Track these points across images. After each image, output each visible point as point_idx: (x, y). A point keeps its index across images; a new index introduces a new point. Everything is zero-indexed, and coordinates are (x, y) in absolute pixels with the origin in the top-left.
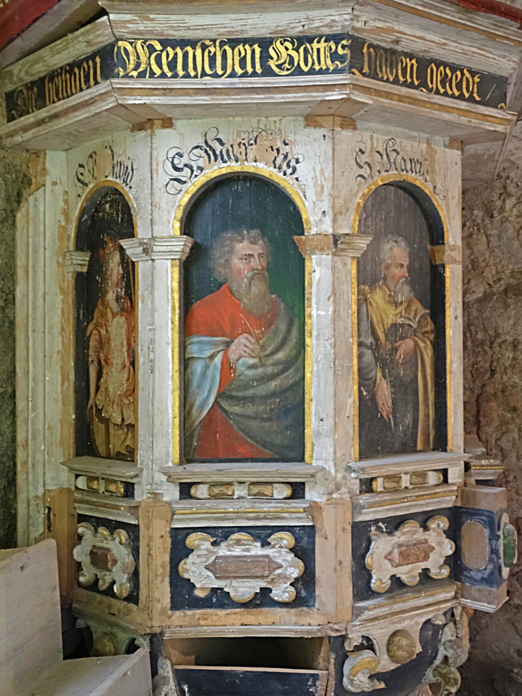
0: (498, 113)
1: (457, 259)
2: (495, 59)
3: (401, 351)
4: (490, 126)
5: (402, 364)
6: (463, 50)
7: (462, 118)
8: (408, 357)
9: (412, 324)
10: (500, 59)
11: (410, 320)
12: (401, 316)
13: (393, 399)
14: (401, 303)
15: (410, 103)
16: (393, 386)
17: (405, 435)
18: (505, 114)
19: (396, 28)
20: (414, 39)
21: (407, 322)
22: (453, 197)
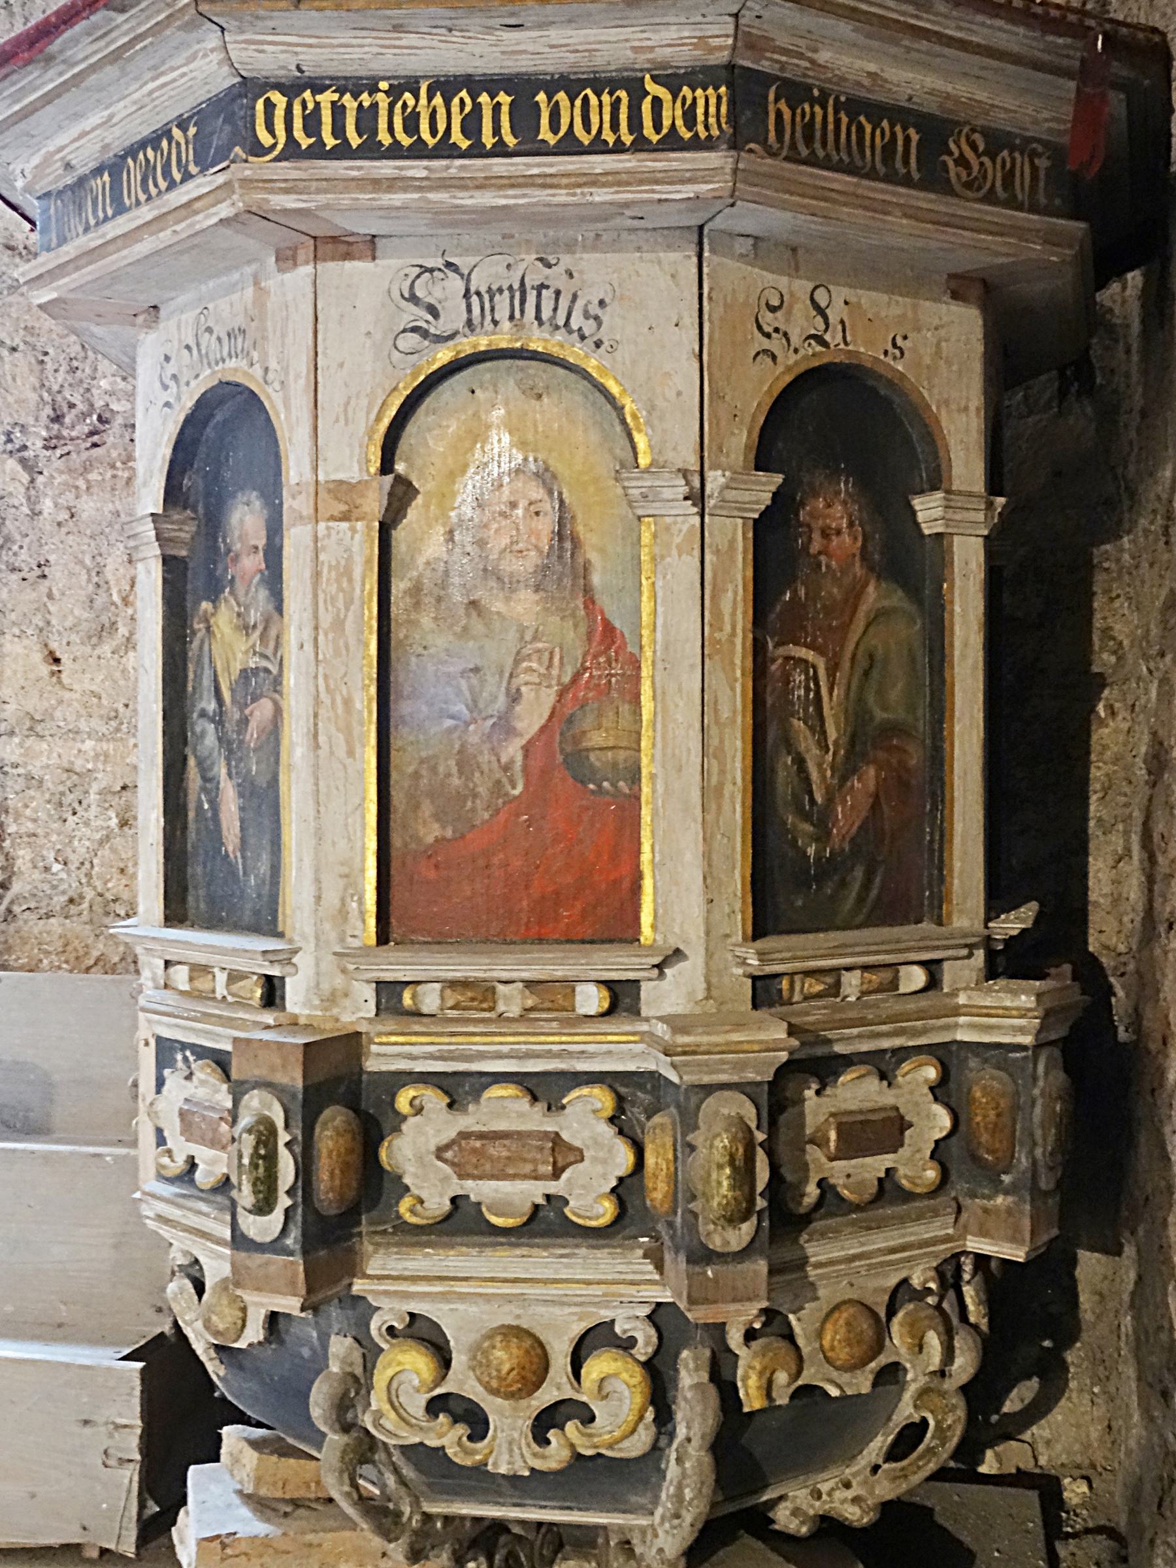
0: (198, 186)
1: (305, 513)
2: (184, 75)
3: (253, 725)
4: (207, 217)
5: (255, 750)
6: (135, 103)
7: (161, 235)
8: (264, 738)
9: (270, 667)
10: (192, 66)
11: (266, 657)
12: (255, 653)
13: (242, 821)
14: (255, 626)
15: (90, 263)
16: (241, 795)
17: (259, 896)
18: (208, 178)
19: (51, 149)
20: (77, 144)
21: (264, 664)
22: (298, 376)
